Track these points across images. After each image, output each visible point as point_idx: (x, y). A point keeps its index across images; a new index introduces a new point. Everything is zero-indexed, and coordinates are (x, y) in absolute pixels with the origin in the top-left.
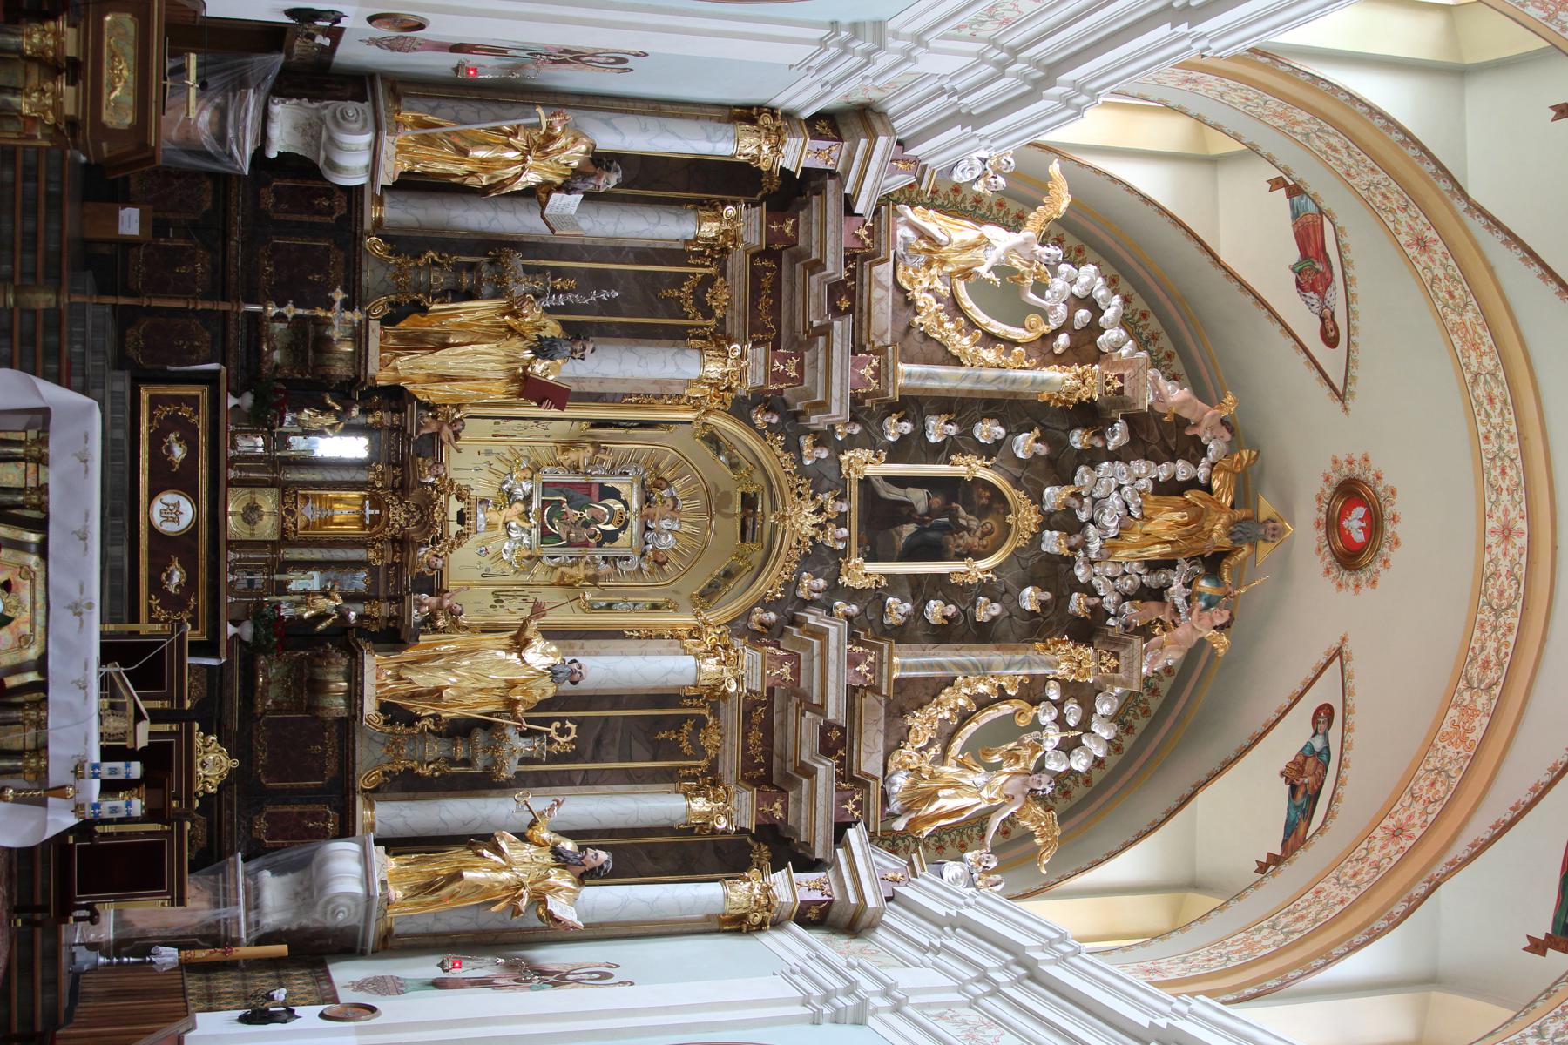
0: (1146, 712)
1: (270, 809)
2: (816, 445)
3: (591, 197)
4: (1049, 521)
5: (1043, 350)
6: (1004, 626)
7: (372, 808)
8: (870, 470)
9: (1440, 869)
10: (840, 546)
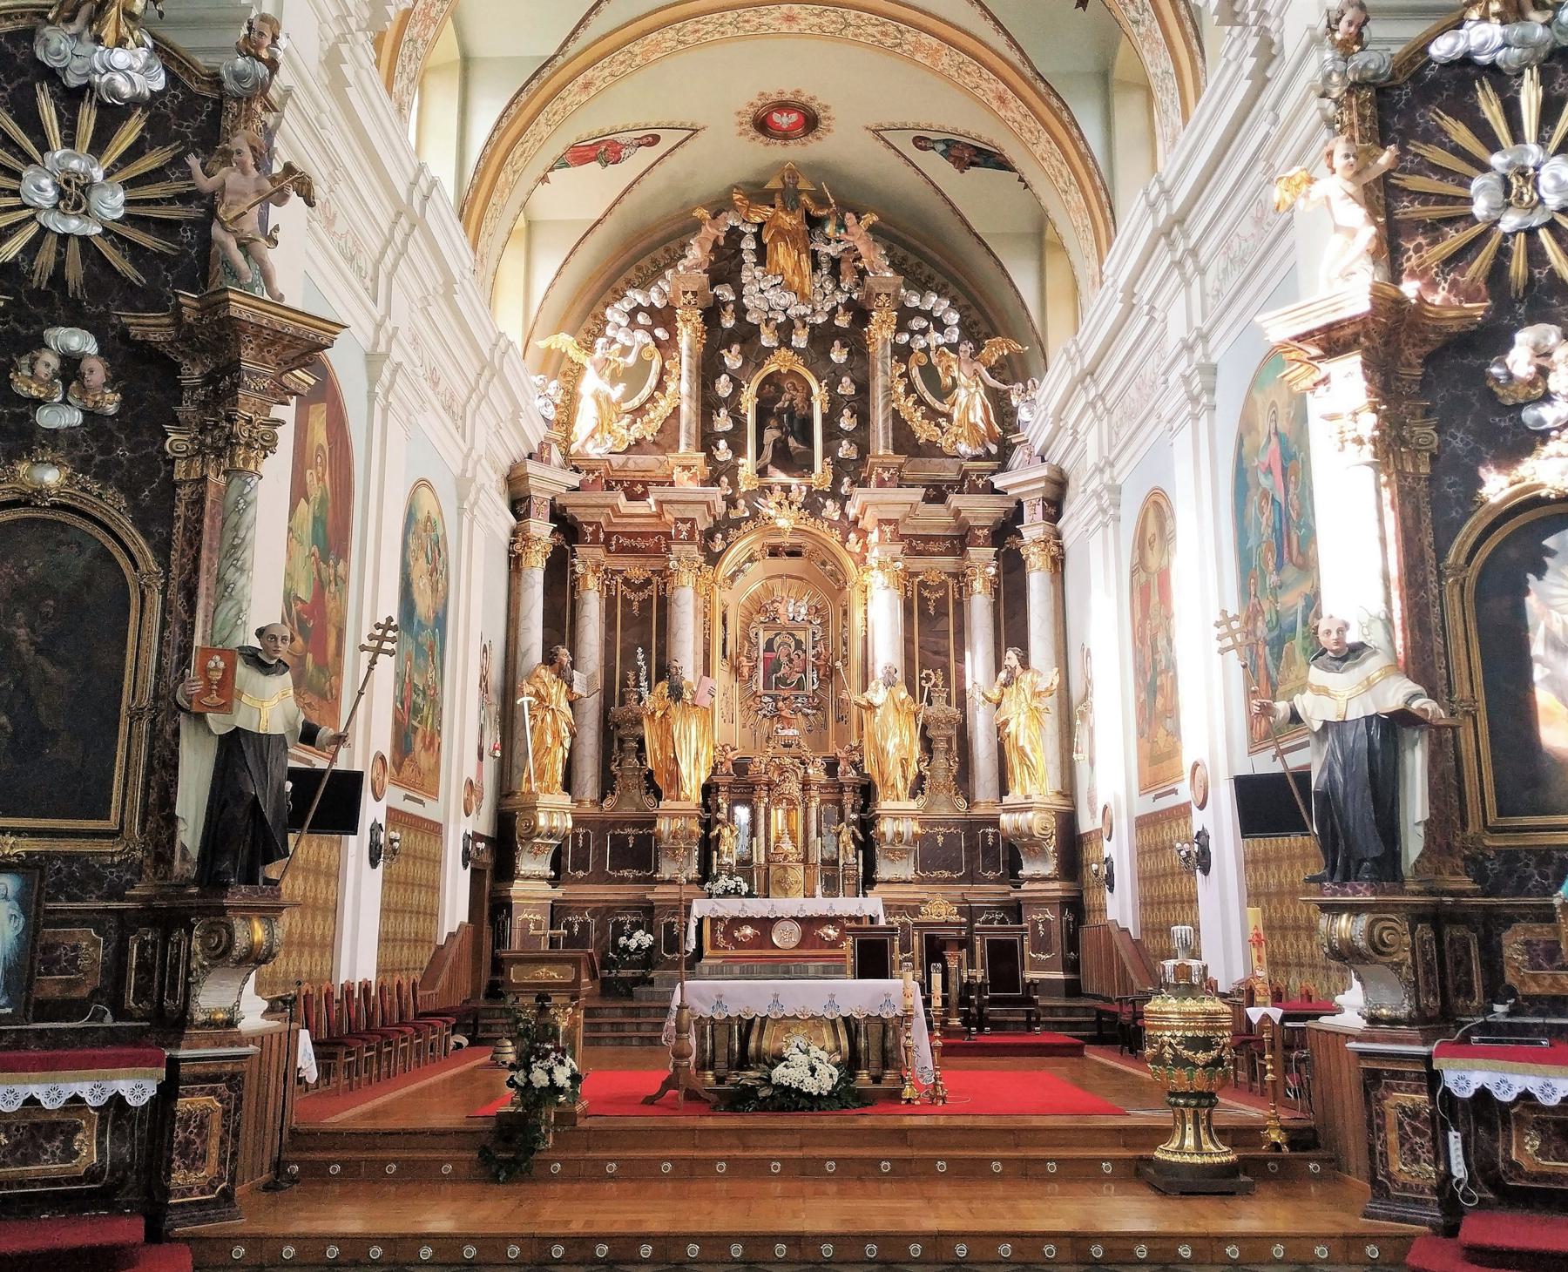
0: (919, 265)
2: (735, 508)
3: (573, 665)
4: (785, 342)
5: (666, 347)
6: (858, 374)
10: (804, 488)
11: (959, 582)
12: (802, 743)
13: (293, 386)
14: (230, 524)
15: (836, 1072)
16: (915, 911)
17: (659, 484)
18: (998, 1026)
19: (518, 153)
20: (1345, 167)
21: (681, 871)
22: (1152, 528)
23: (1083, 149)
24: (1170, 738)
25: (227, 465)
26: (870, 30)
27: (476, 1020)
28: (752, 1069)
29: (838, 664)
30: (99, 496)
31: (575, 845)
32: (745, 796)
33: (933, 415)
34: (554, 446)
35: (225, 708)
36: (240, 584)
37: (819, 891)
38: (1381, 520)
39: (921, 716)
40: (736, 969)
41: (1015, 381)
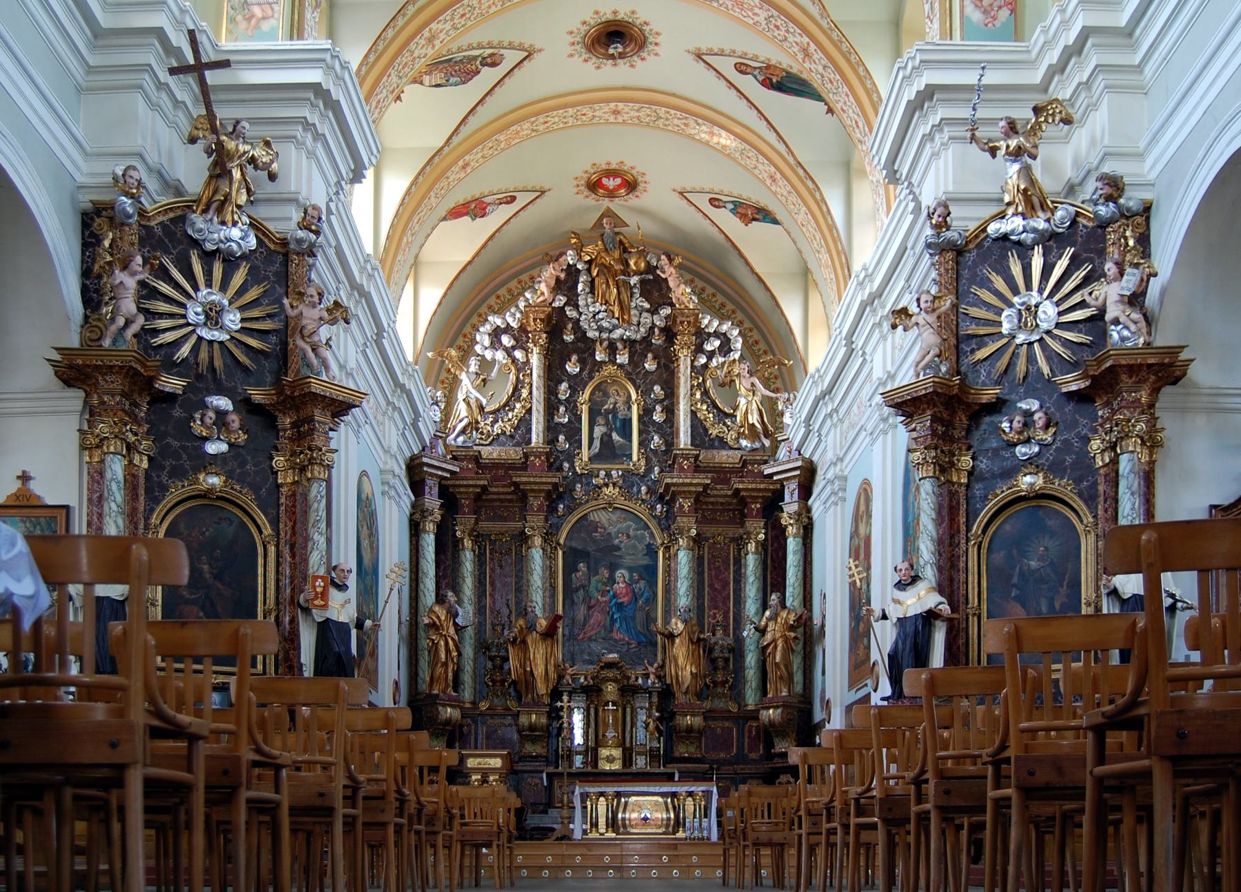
1: (746, 751)
8: (585, 458)
9: (791, 160)
23: (830, 222)
26: (676, 121)
30: (240, 492)
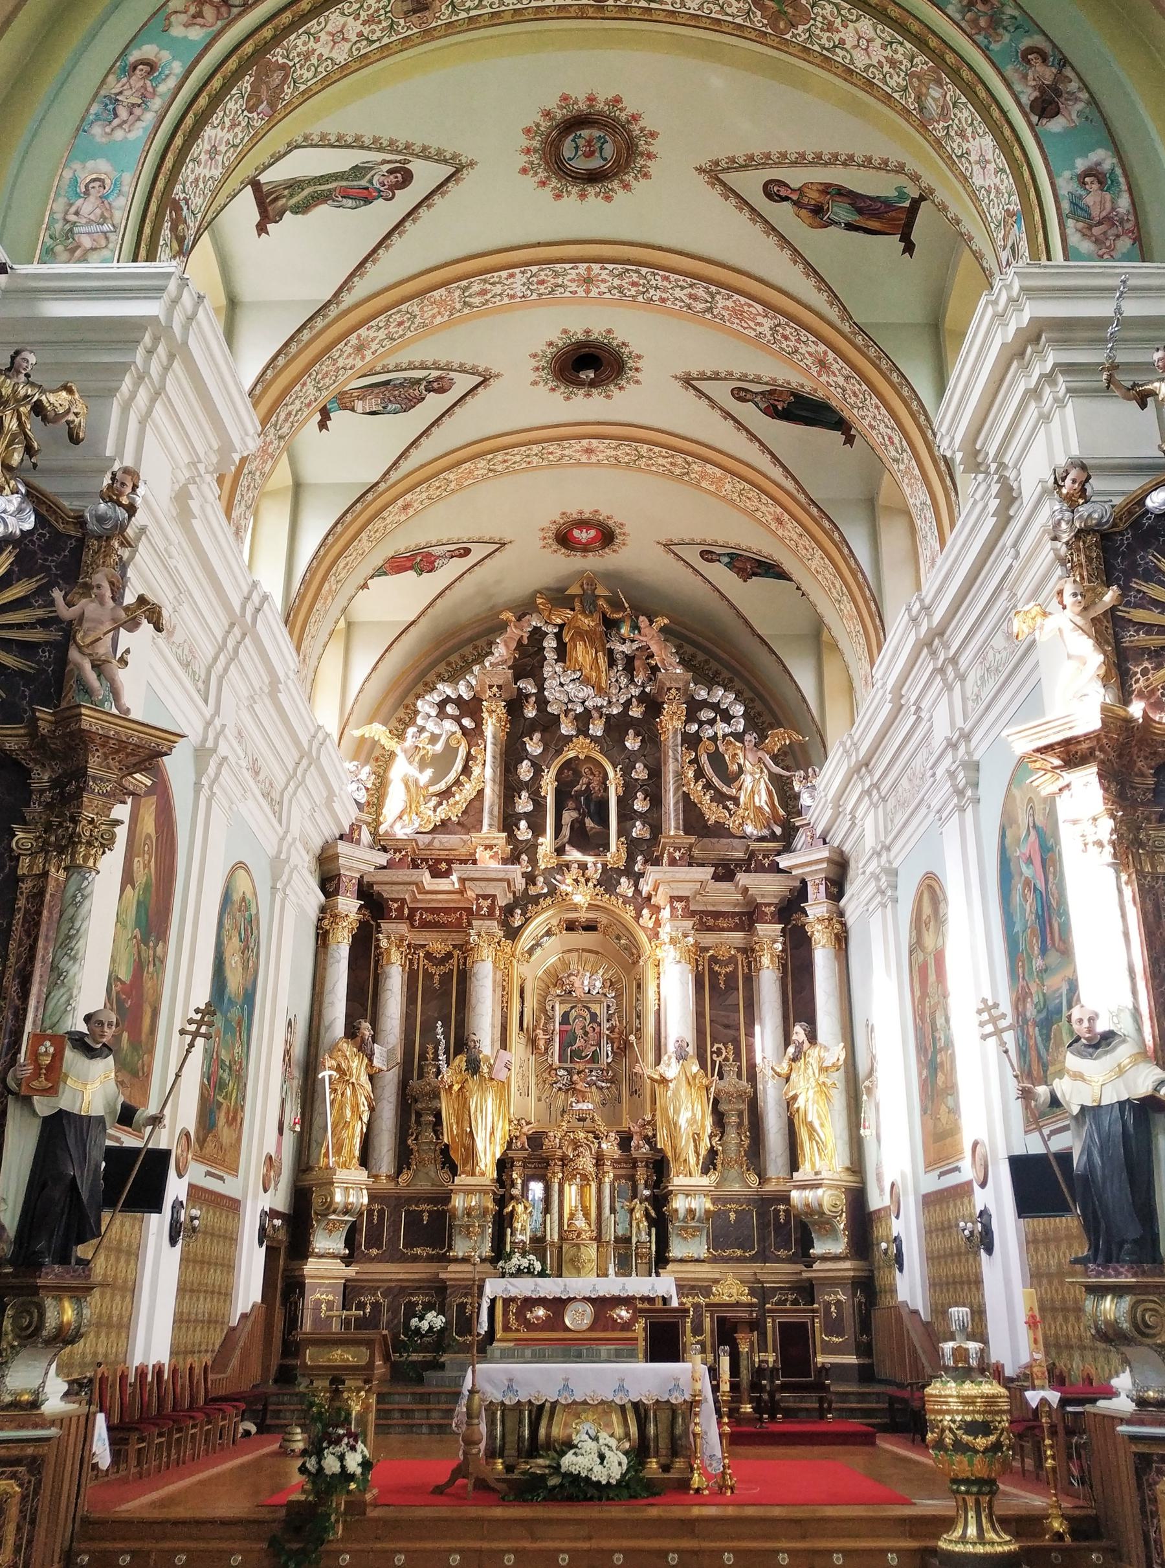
0: (706, 662)
2: (535, 884)
3: (374, 1039)
4: (583, 731)
5: (473, 735)
7: (770, 1179)
10: (599, 866)
11: (747, 957)
12: (596, 1117)
13: (131, 788)
14: (66, 916)
15: (625, 1461)
16: (707, 1291)
17: (465, 862)
18: (789, 1414)
19: (341, 566)
20: (1074, 604)
21: (474, 1249)
22: (927, 910)
24: (952, 1115)
25: (68, 862)
26: (661, 461)
27: (265, 1406)
28: (541, 1457)
29: (632, 1038)
31: (370, 1220)
32: (539, 1172)
33: (720, 798)
34: (364, 827)
35: (52, 1091)
36: (71, 973)
37: (611, 1271)
38: (1124, 916)
39: (712, 1089)
40: (528, 1353)
41: (798, 769)
